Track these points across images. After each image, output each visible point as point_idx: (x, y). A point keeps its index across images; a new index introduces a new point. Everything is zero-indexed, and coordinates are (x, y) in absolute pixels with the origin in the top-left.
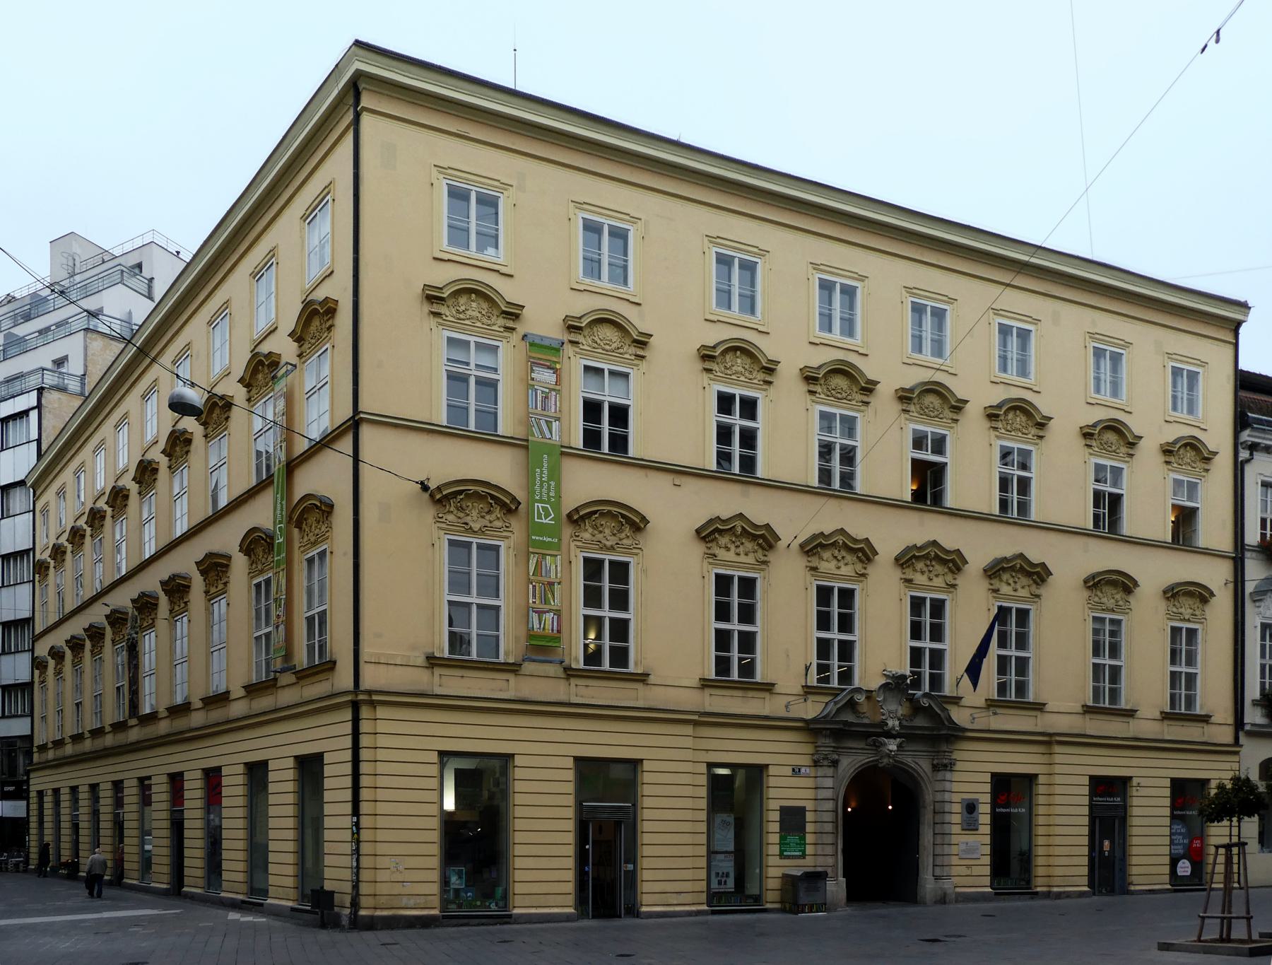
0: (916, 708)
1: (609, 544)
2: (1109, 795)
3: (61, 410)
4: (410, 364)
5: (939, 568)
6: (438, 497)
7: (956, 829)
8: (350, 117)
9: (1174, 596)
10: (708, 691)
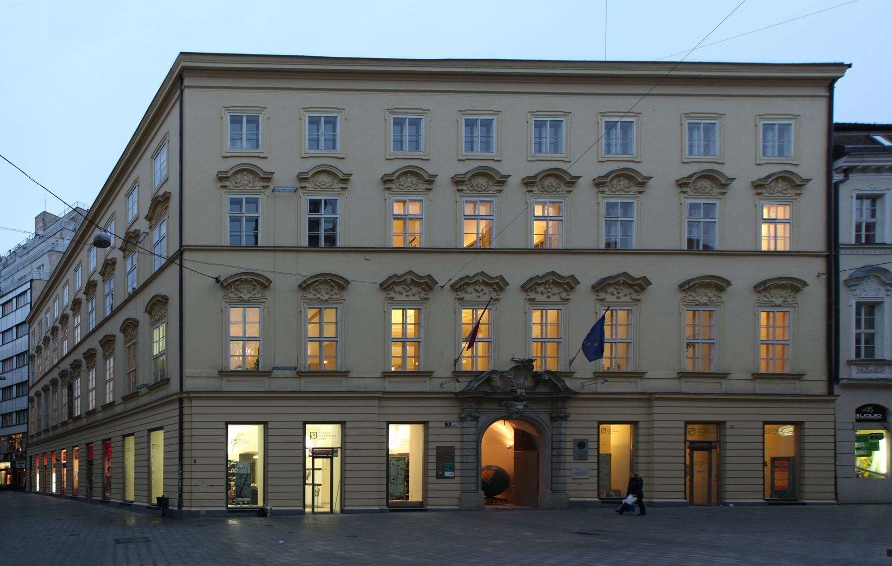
1: (324, 298)
3: (39, 288)
4: (208, 217)
7: (570, 459)
8: (178, 93)
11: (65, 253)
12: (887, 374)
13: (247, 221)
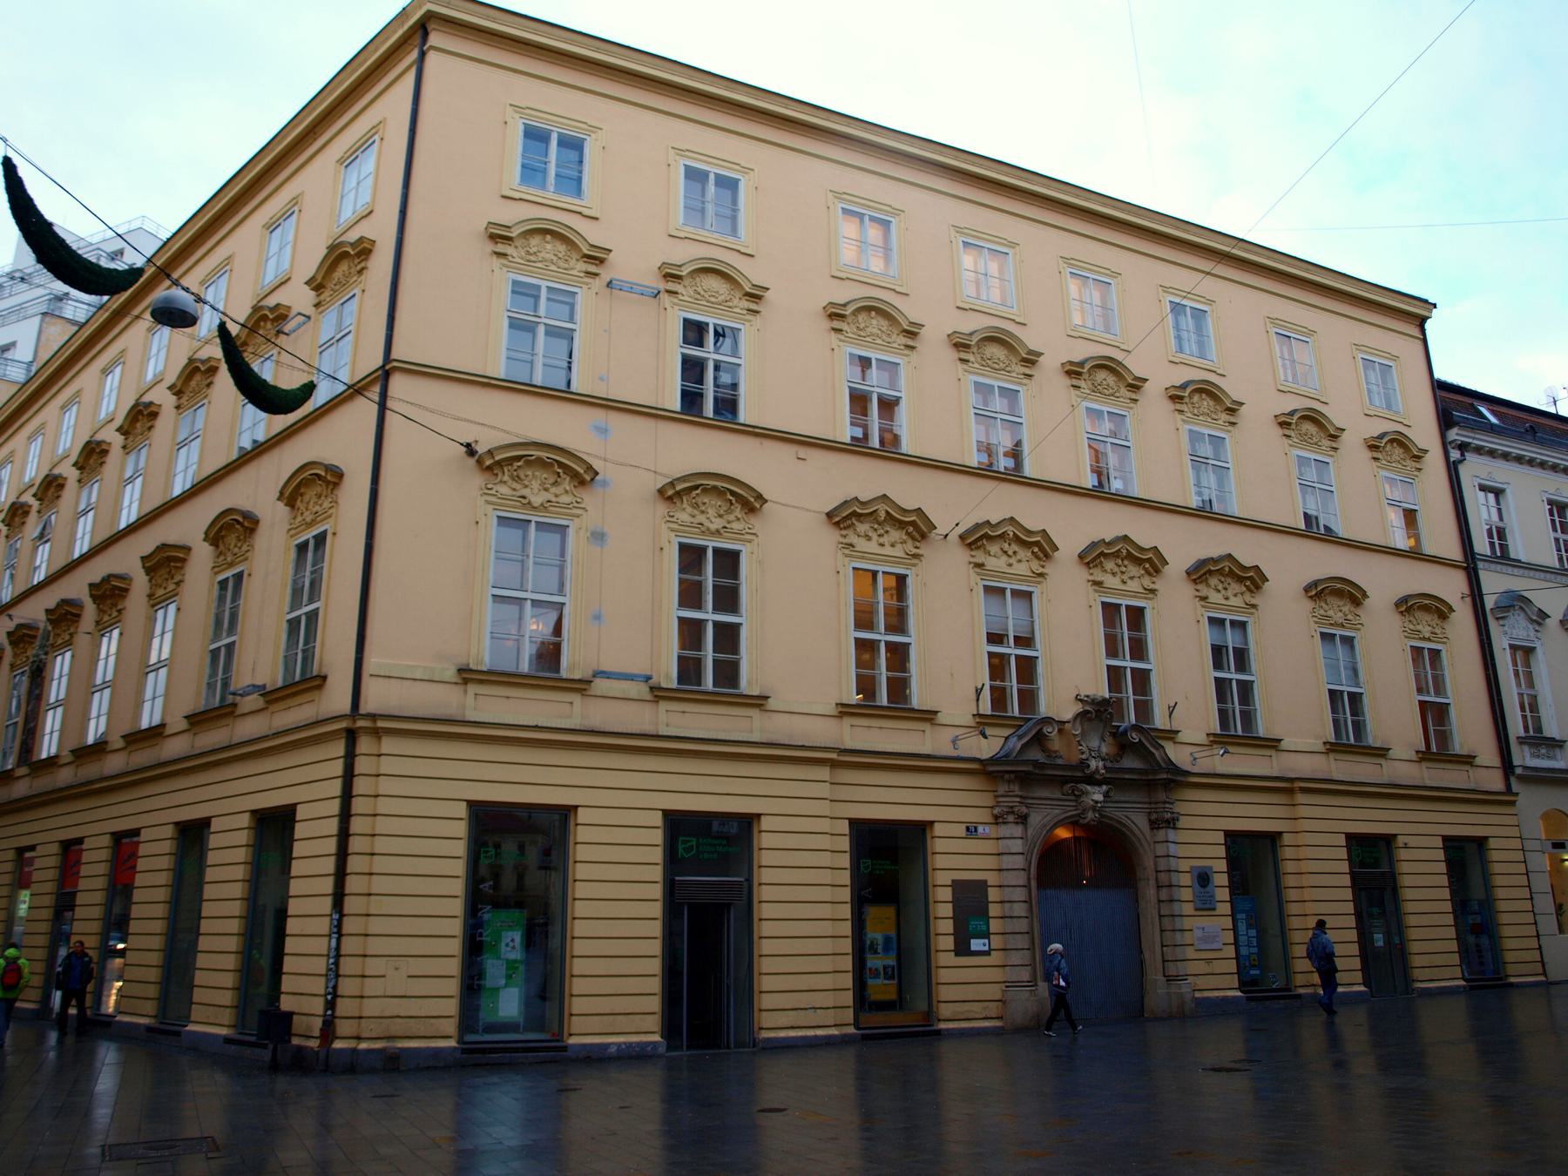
1: (713, 527)
2: (1371, 860)
4: (459, 309)
5: (1133, 570)
6: (488, 462)
7: (1188, 909)
8: (415, 54)
9: (1409, 610)
10: (848, 721)
11: (82, 326)
12: (1562, 761)
13: (547, 333)
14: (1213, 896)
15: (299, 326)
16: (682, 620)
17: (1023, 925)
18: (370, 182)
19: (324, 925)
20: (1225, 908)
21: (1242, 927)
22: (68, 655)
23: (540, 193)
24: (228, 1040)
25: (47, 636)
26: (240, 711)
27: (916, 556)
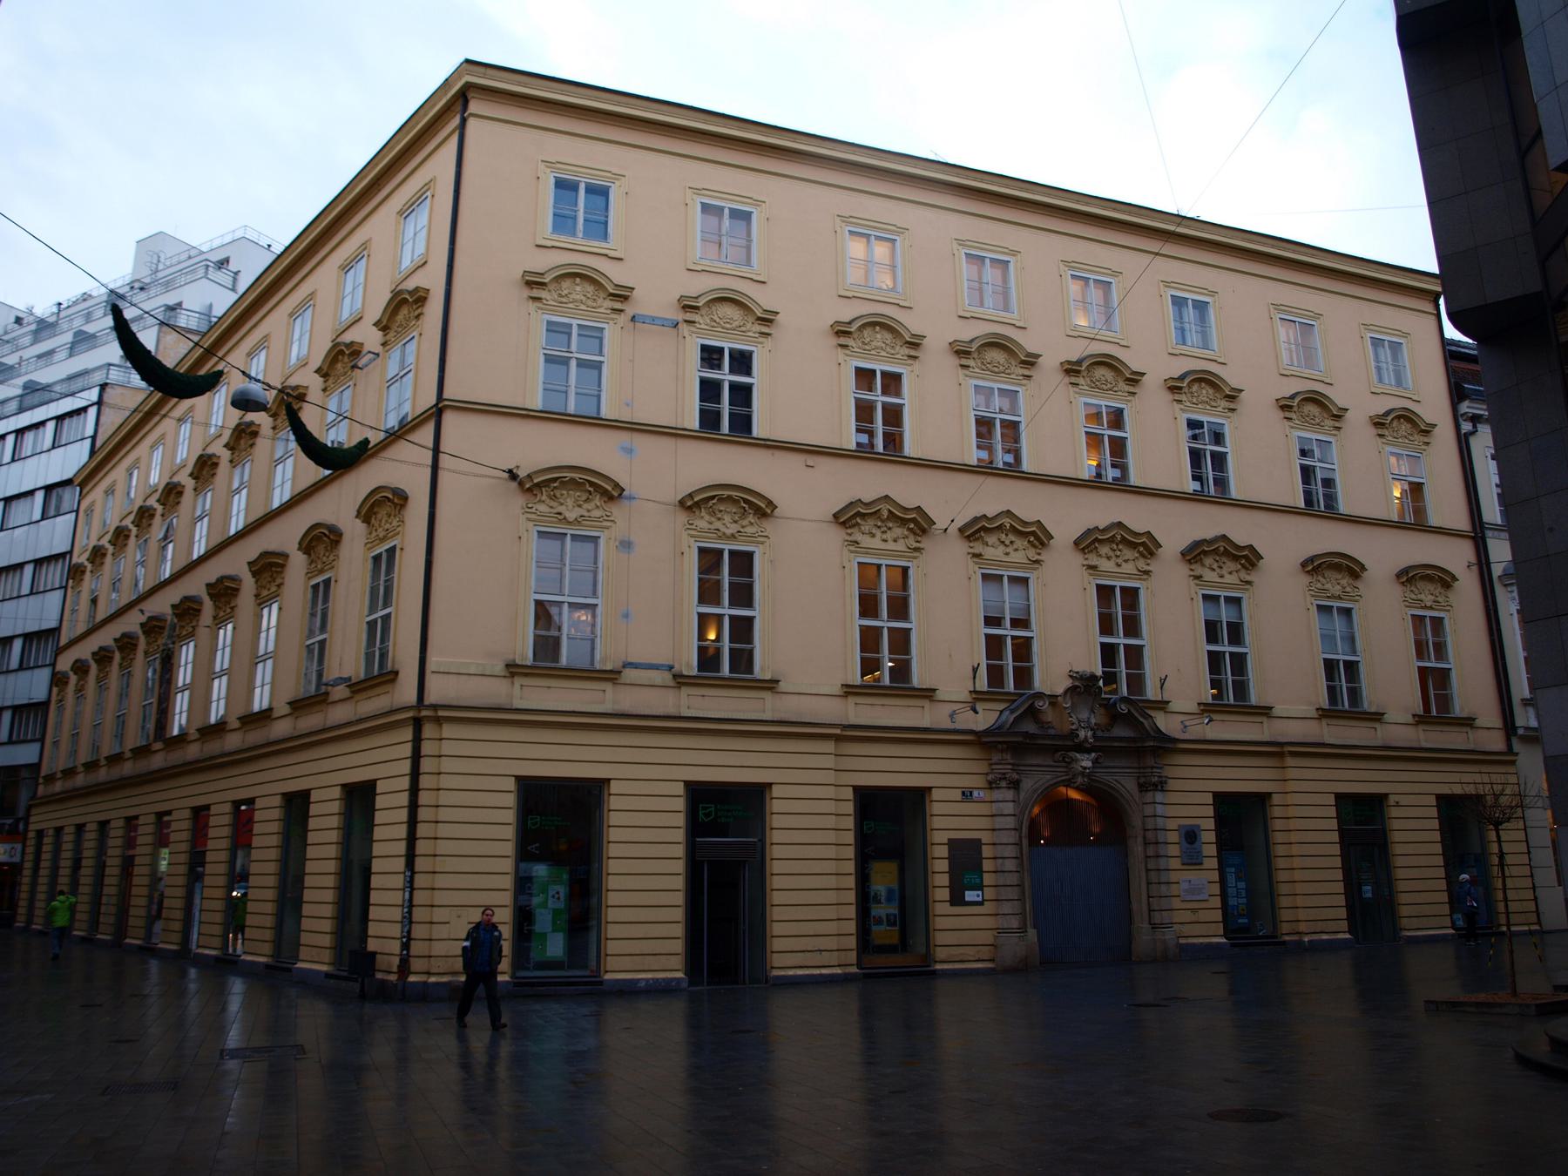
0: (1114, 717)
1: (728, 532)
2: (1362, 820)
4: (501, 350)
5: (1128, 553)
7: (1175, 863)
8: (456, 121)
10: (851, 700)
14: (1200, 852)
15: (371, 361)
16: (1102, 644)
17: (1013, 879)
18: (424, 234)
19: (399, 881)
20: (1214, 863)
21: (1231, 880)
22: (192, 645)
23: (571, 239)
24: (327, 975)
25: (173, 628)
26: (331, 699)
27: (917, 549)
